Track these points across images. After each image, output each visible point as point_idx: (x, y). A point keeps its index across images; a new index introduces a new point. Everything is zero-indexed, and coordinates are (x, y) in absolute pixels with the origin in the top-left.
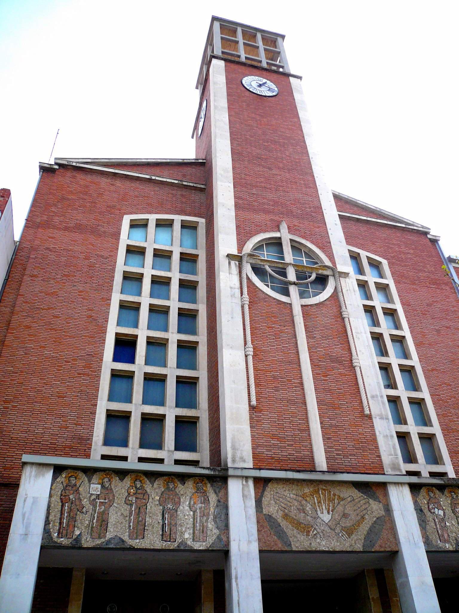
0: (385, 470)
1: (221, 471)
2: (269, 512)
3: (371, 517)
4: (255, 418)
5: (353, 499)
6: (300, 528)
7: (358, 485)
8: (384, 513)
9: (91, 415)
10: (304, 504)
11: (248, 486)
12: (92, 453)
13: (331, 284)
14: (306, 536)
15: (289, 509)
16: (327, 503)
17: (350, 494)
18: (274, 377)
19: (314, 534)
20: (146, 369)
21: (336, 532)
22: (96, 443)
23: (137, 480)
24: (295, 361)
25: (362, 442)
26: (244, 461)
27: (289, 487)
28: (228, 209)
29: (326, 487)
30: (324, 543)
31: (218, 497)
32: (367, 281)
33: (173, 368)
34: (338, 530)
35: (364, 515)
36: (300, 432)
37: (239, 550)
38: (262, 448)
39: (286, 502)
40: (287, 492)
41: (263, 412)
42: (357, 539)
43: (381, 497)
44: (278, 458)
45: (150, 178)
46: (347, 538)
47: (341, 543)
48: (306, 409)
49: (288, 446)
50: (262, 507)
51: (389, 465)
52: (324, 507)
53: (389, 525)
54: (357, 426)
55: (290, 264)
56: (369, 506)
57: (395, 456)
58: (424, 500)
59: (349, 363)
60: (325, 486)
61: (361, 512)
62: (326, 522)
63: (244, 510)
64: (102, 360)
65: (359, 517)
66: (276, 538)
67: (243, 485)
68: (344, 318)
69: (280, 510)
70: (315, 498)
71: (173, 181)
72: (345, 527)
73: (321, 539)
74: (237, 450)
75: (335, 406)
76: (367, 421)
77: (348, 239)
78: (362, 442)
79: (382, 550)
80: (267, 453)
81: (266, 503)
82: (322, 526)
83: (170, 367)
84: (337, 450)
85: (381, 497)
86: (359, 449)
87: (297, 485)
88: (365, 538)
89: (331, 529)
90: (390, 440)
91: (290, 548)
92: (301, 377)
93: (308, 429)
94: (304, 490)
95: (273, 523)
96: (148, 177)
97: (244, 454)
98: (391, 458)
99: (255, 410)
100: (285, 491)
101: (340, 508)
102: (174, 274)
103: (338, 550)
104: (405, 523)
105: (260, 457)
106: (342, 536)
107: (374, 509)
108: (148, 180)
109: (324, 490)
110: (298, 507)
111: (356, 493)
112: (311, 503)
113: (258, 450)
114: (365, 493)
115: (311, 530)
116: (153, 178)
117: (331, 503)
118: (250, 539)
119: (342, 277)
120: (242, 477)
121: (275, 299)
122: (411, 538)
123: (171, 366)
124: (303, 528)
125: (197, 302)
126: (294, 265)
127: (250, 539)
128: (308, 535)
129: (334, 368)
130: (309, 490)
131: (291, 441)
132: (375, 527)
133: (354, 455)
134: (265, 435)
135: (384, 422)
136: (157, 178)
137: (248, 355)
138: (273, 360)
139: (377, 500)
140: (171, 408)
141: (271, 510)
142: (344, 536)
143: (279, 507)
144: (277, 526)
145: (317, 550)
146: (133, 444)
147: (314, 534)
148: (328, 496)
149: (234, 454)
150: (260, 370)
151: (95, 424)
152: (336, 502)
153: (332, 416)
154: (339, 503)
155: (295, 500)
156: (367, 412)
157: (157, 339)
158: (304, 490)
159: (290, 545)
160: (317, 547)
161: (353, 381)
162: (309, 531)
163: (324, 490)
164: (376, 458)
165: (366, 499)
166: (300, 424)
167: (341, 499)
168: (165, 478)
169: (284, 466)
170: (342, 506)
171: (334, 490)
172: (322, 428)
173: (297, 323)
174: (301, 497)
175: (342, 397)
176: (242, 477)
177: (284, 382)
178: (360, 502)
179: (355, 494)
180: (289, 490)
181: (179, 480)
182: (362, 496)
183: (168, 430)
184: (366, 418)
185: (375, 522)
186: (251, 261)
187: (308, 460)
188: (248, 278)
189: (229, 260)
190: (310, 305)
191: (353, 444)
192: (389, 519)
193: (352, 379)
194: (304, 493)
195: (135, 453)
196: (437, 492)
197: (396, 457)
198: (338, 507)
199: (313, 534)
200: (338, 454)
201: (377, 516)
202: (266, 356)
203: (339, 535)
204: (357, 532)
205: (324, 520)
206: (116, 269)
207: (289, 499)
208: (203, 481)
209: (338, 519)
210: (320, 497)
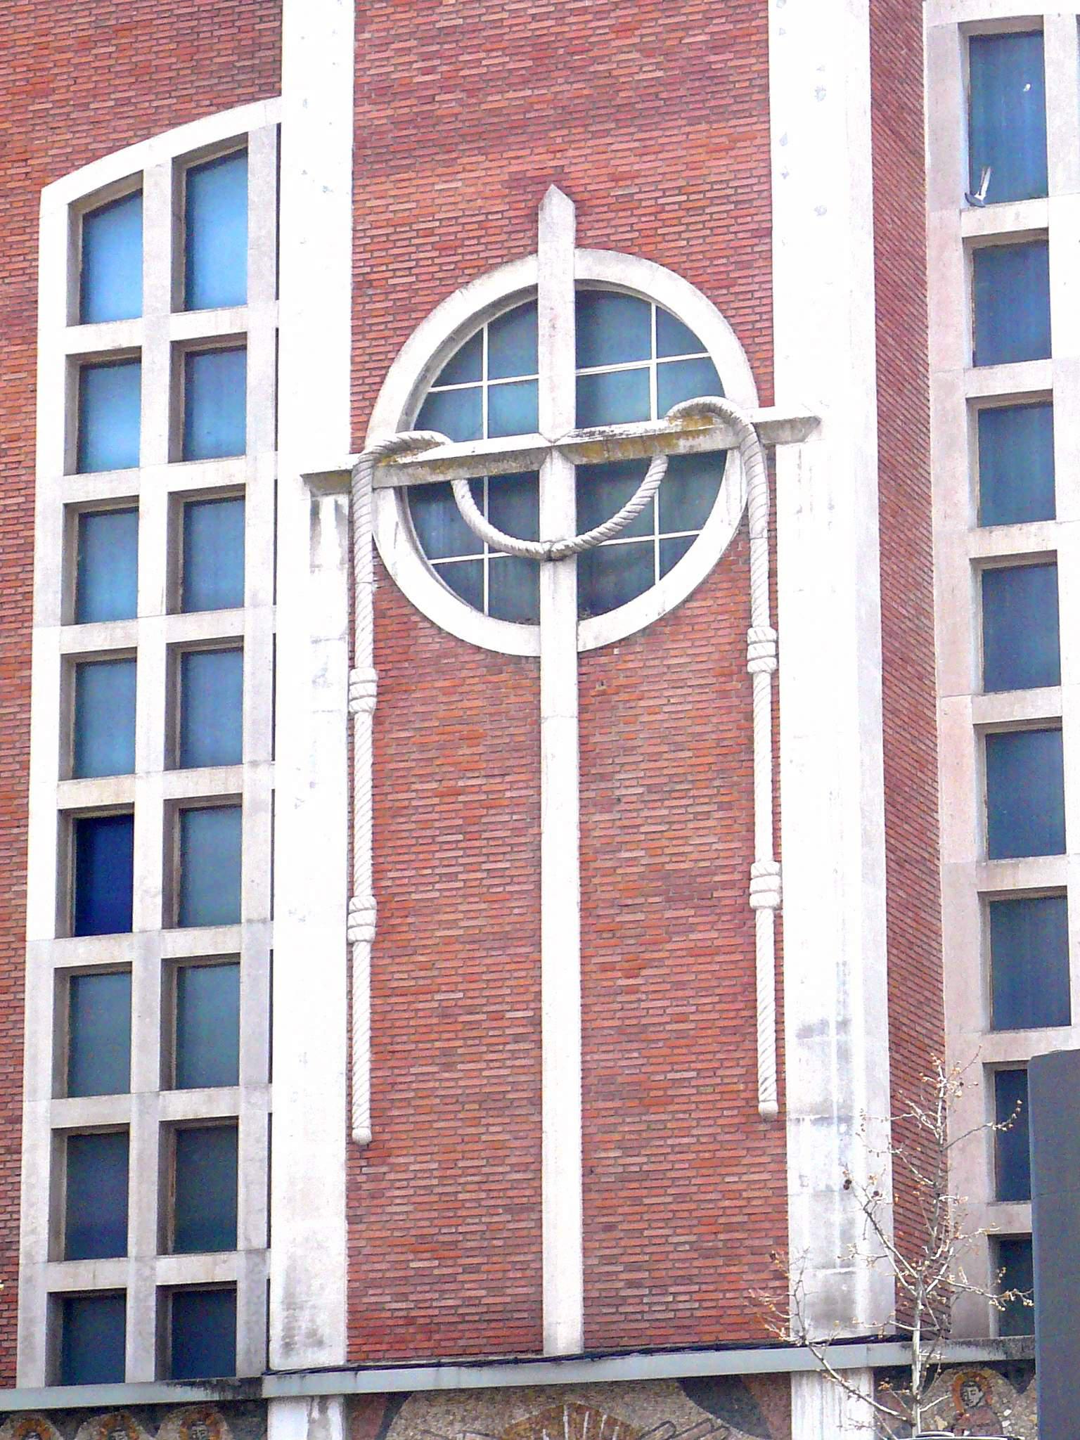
1: (240, 1387)
7: (694, 1387)
9: (9, 1158)
11: (325, 1424)
12: (20, 1292)
17: (667, 1417)
18: (445, 1013)
20: (169, 948)
22: (29, 1256)
23: (29, 1432)
25: (730, 1227)
26: (320, 1343)
27: (466, 1411)
40: (458, 1426)
51: (813, 1305)
57: (842, 1267)
58: (937, 1418)
64: (23, 939)
67: (311, 1421)
74: (301, 1308)
78: (730, 1227)
83: (250, 921)
90: (837, 1205)
97: (319, 1321)
98: (826, 1281)
99: (369, 1154)
100: (451, 1423)
102: (256, 459)
109: (579, 1410)
111: (689, 1413)
113: (365, 1300)
123: (251, 917)
125: (124, 812)
126: (566, 451)
133: (689, 1280)
138: (448, 941)
139: (759, 1431)
146: (139, 1243)
149: (289, 1322)
150: (395, 992)
151: (23, 1187)
156: (768, 1105)
158: (510, 1416)
168: (105, 1417)
169: (443, 1344)
171: (612, 1409)
172: (586, 1188)
179: (683, 1417)
180: (463, 1420)
181: (141, 1422)
182: (708, 1420)
183: (246, 1176)
188: (381, 573)
189: (313, 495)
191: (693, 1238)
195: (147, 1272)
196: (1000, 1383)
200: (631, 1284)
206: (39, 506)
208: (208, 1415)
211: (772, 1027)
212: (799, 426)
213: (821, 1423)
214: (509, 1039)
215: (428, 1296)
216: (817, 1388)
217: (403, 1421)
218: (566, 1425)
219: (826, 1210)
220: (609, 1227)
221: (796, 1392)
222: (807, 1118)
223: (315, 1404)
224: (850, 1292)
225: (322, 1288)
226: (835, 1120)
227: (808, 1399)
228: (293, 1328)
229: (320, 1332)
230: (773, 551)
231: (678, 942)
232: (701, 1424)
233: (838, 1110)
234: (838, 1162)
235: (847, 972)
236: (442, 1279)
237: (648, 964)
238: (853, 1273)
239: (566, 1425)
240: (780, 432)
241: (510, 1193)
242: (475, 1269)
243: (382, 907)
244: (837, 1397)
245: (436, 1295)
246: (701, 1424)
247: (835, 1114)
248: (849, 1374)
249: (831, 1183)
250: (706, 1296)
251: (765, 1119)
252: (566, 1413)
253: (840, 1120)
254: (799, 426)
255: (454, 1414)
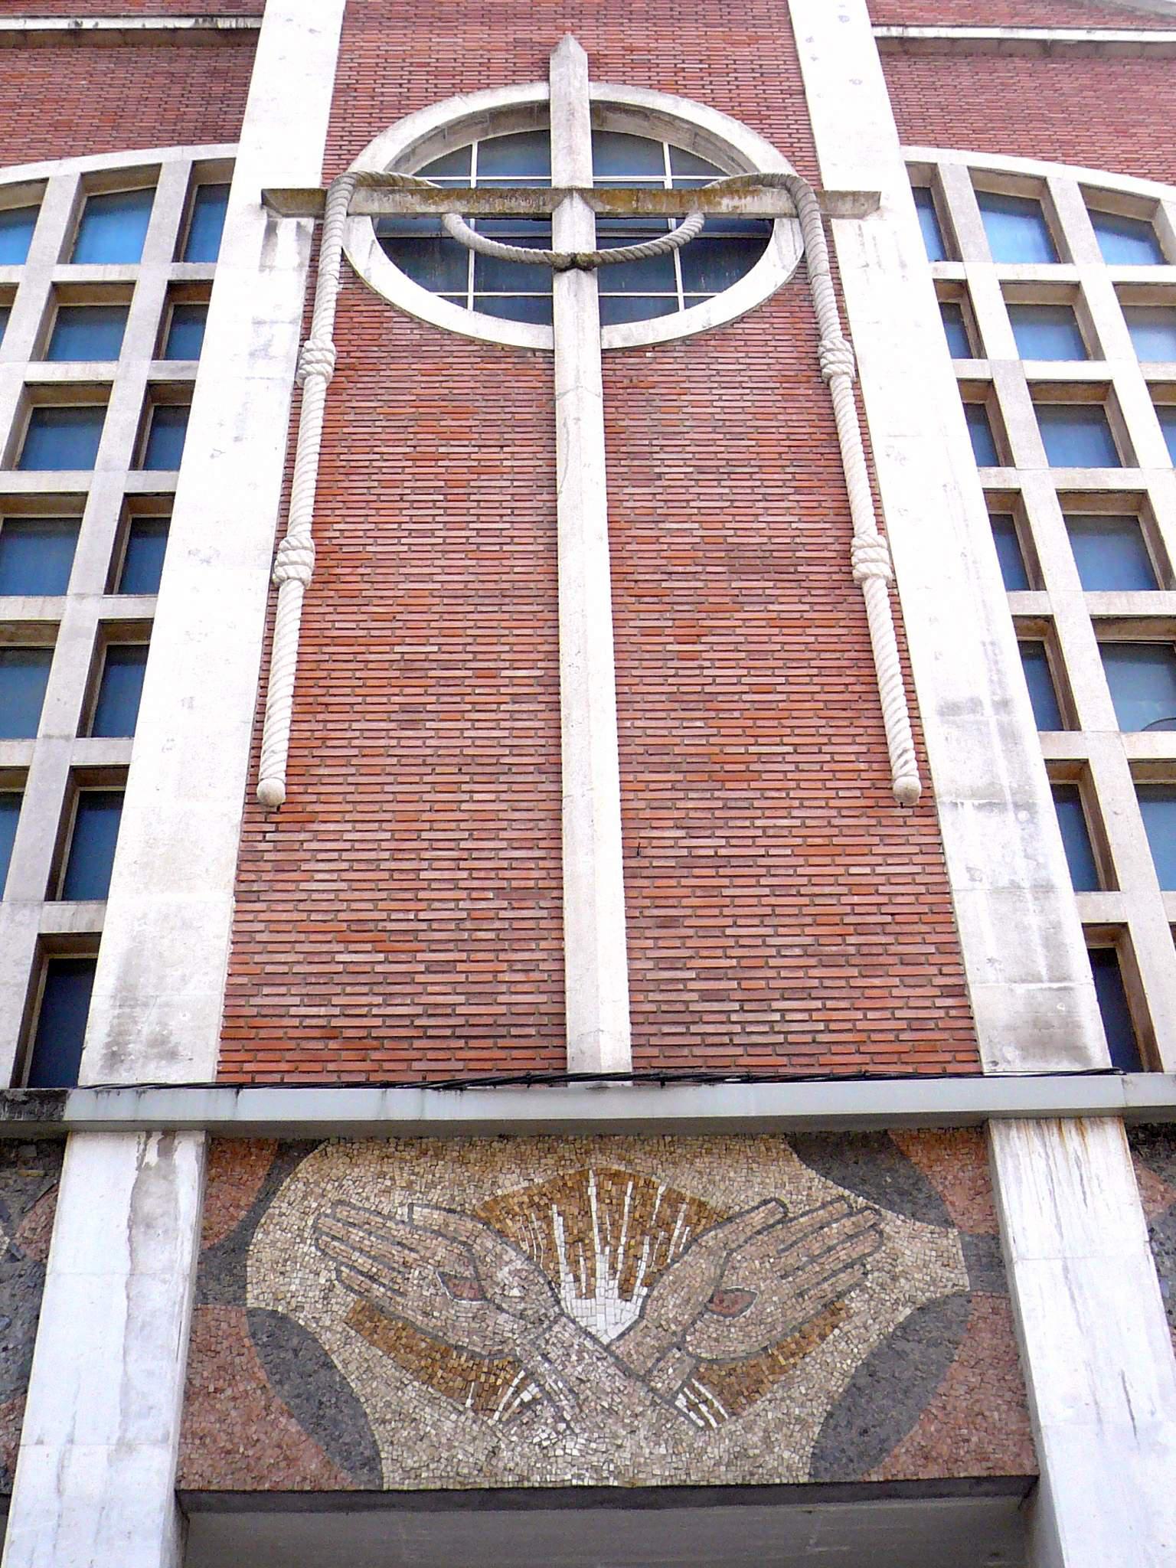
0: (985, 1058)
1: (25, 1103)
2: (277, 1300)
3: (883, 1302)
4: (267, 856)
5: (786, 1214)
6: (440, 1373)
8: (965, 1281)
10: (488, 1251)
11: (167, 1173)
13: (780, 252)
14: (471, 1414)
15: (392, 1280)
16: (623, 1240)
17: (771, 1192)
18: (407, 666)
19: (522, 1403)
21: (653, 1390)
24: (532, 585)
25: (860, 929)
26: (172, 1055)
28: (311, 31)
29: (630, 1162)
30: (573, 1447)
31: (12, 1237)
32: (1076, 286)
33: (61, 737)
34: (667, 1379)
35: (840, 1296)
36: (505, 904)
37: (59, 1492)
38: (283, 990)
39: (382, 1247)
41: (315, 827)
42: (780, 1424)
43: (957, 1199)
44: (362, 1033)
45: (73, 27)
46: (718, 1416)
47: (678, 1442)
48: (558, 796)
49: (428, 971)
50: (245, 1277)
51: (1011, 1028)
52: (602, 1266)
53: (986, 1338)
54: (845, 850)
55: (569, 191)
56: (877, 1249)
57: (1051, 981)
59: (836, 569)
60: (621, 1158)
61: (825, 1279)
62: (605, 1340)
63: (127, 1285)
65: (810, 1307)
66: (294, 1427)
68: (830, 377)
69: (339, 1289)
70: (558, 1221)
71: (171, 23)
72: (712, 1361)
73: (562, 1426)
74: (146, 1005)
75: (728, 767)
76: (905, 825)
77: (993, 129)
78: (860, 929)
79: (934, 1472)
80: (303, 1011)
81: (267, 1255)
82: (574, 1358)
83: (48, 737)
84: (705, 973)
85: (957, 1199)
86: (842, 961)
87: (463, 1162)
88: (830, 1415)
89: (628, 1373)
90: (1031, 905)
91: (365, 1478)
92: (554, 656)
93: (554, 884)
94: (494, 1183)
95: (290, 1355)
96: (65, 26)
97: (173, 1024)
98: (1030, 996)
99: (278, 818)
100: (387, 1191)
101: (698, 1268)
103: (654, 1482)
104: (1079, 1325)
105: (263, 1033)
106: (692, 1407)
107: (908, 1260)
108: (66, 39)
109: (616, 1177)
110: (447, 1270)
112: (525, 1246)
114: (864, 1181)
115: (507, 1383)
116: (88, 24)
117: (647, 1239)
118: (129, 1435)
119: (842, 217)
120: (143, 1129)
121: (471, 341)
122: (1112, 1400)
124: (463, 1373)
127: (129, 1435)
128: (483, 1408)
129: (741, 599)
130: (526, 1184)
131: (451, 946)
132: (901, 1355)
134: (312, 927)
135: (1007, 826)
136: (105, 24)
137: (282, 581)
140: (25, 906)
141: (293, 1288)
142: (703, 1408)
143: (338, 1272)
144: (310, 1366)
145: (526, 1484)
147: (522, 1403)
148: (633, 1208)
152: (676, 1233)
153: (699, 814)
154: (694, 1240)
155: (438, 1233)
156: (906, 778)
157: (13, 629)
159: (372, 1462)
160: (531, 1468)
161: (848, 647)
162: (494, 1389)
163: (616, 1177)
164: (939, 1002)
165: (861, 1211)
166: (512, 864)
167: (704, 1216)
170: (711, 1252)
171: (674, 1178)
172: (629, 874)
173: (565, 424)
174: (474, 1217)
175: (775, 723)
176: (143, 1129)
177: (458, 681)
178: (822, 1228)
179: (799, 1193)
182: (842, 1198)
184: (898, 812)
185: (903, 1327)
186: (375, 207)
187: (532, 1031)
190: (654, 347)
192: (995, 1311)
193: (843, 638)
194: (495, 1200)
197: (1056, 985)
198: (686, 1258)
199: (517, 1402)
200: (706, 996)
201: (922, 1298)
202: (381, 578)
203: (671, 1403)
204: (788, 1386)
205: (593, 1330)
207: (401, 1232)
209: (675, 1320)
210: (587, 1213)
211: (902, 701)
212: (862, 200)
213: (1052, 1192)
214: (507, 699)
215: (364, 1000)
216: (1036, 1142)
217: (300, 1185)
218: (593, 1200)
219: (1016, 910)
220: (667, 923)
221: (1002, 1149)
222: (968, 803)
223: (156, 1137)
224: (1070, 1012)
225: (184, 979)
226: (1010, 807)
227: (1024, 1160)
228: (127, 1033)
229: (173, 1039)
230: (839, 293)
231: (751, 611)
232: (831, 1203)
233: (1013, 794)
234: (1023, 854)
235: (997, 651)
236: (387, 978)
237: (712, 631)
238: (1071, 989)
239: (593, 1200)
240: (839, 204)
241: (508, 874)
242: (449, 967)
243: (321, 555)
244: (1072, 1156)
245: (379, 1000)
246: (831, 1203)
247: (1009, 798)
248: (1086, 1122)
249: (1017, 879)
250: (835, 1015)
251: (905, 800)
252: (592, 1182)
253: (1017, 806)
254: (862, 200)
255: (392, 1179)
